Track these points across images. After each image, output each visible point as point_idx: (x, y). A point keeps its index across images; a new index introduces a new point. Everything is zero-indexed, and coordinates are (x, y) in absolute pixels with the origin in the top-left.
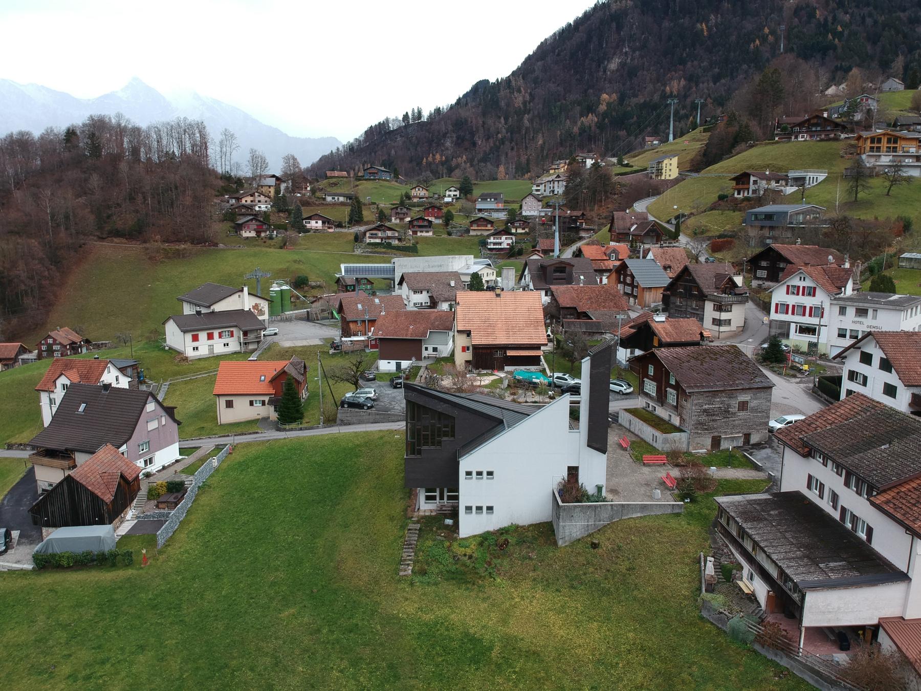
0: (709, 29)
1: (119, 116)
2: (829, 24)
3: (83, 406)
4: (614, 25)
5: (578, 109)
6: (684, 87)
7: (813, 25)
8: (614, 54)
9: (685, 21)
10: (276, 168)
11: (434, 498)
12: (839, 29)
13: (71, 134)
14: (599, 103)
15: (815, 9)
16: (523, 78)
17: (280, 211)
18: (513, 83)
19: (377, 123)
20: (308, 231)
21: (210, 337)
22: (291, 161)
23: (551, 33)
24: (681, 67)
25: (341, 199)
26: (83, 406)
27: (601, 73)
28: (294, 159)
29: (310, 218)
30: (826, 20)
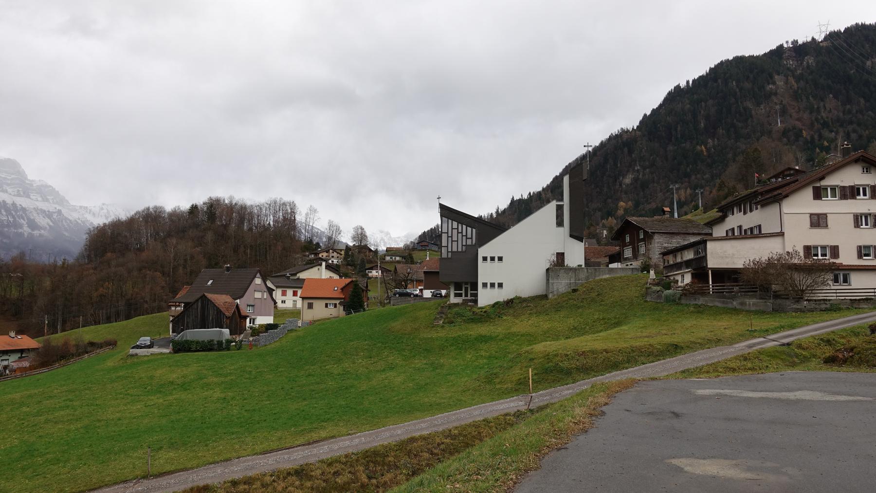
0: (708, 150)
1: (231, 198)
2: (816, 141)
3: (211, 282)
4: (626, 150)
5: (599, 214)
6: (690, 195)
7: (801, 143)
8: (628, 171)
9: (687, 145)
10: (347, 239)
11: (460, 295)
12: (826, 144)
13: (194, 209)
14: (617, 209)
15: (801, 130)
16: (552, 192)
17: (348, 265)
18: (543, 196)
19: (429, 229)
20: (370, 278)
21: (295, 294)
22: (360, 231)
23: (574, 159)
24: (687, 179)
25: (398, 258)
26: (211, 282)
27: (617, 187)
28: (362, 229)
29: (372, 268)
30: (812, 137)
